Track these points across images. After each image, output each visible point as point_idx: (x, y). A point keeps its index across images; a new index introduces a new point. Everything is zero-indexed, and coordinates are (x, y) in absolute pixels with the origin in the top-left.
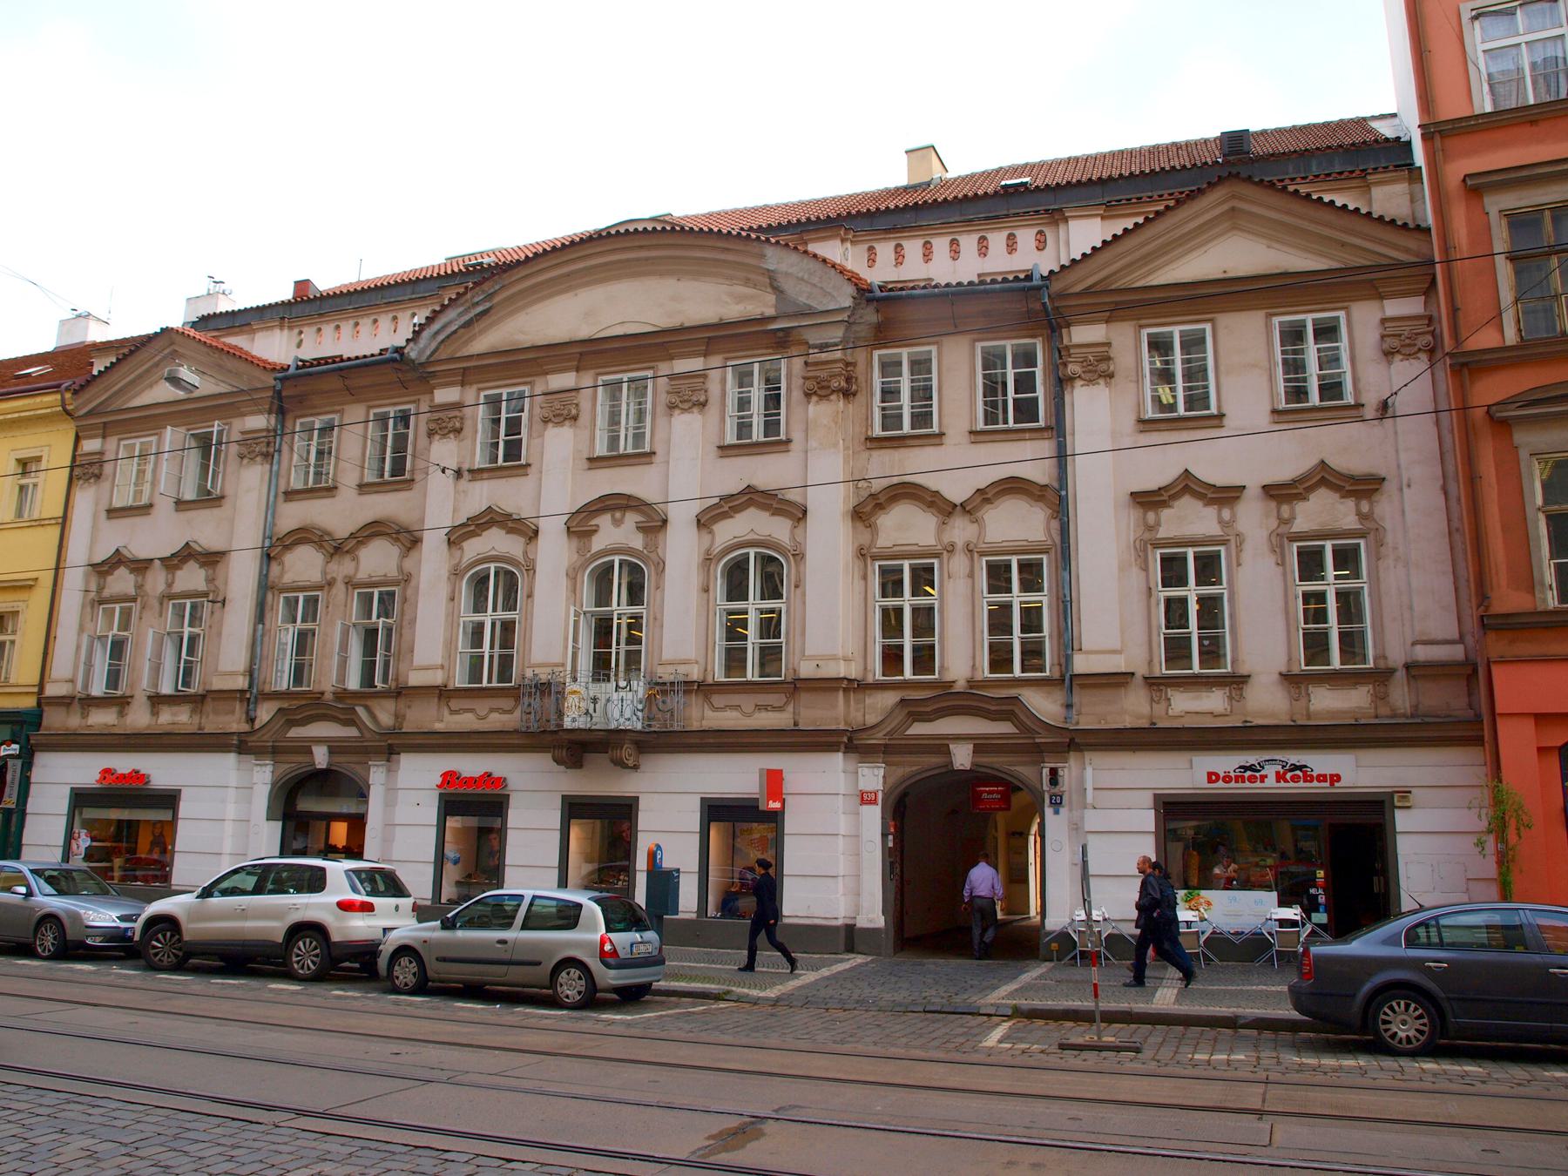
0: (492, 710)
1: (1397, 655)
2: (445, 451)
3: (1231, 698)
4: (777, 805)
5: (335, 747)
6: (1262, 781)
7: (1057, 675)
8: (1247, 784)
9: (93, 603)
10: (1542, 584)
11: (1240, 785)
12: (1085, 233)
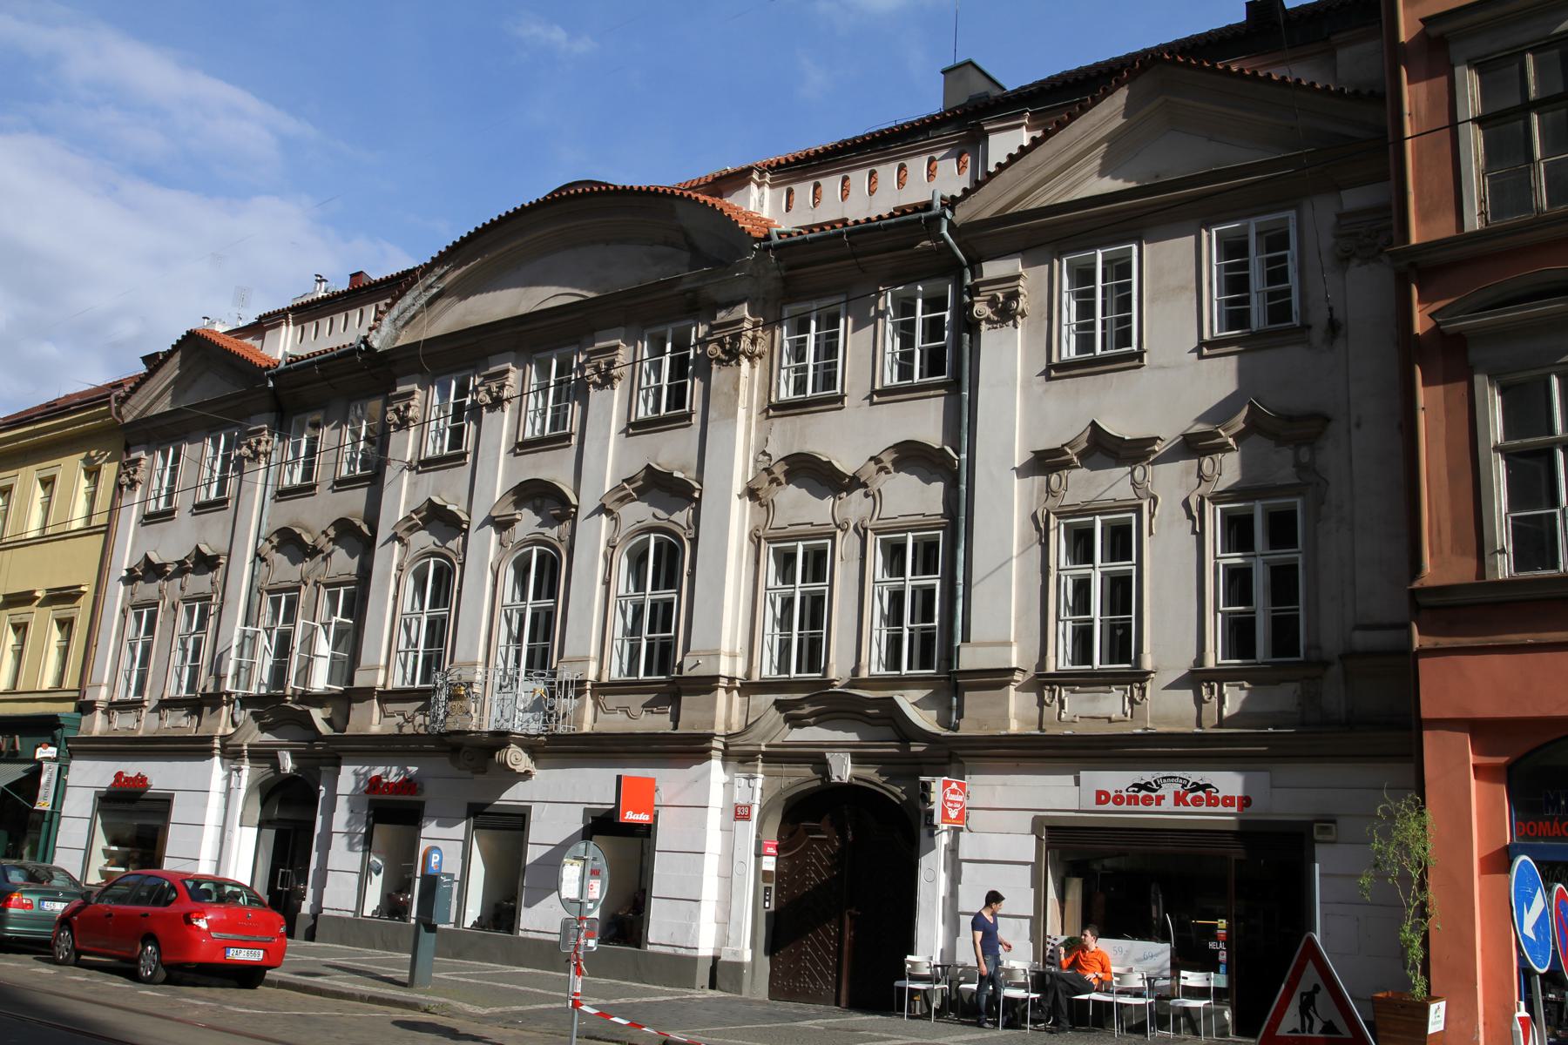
1: (1331, 644)
4: (644, 818)
6: (1158, 804)
8: (1141, 807)
11: (1133, 808)
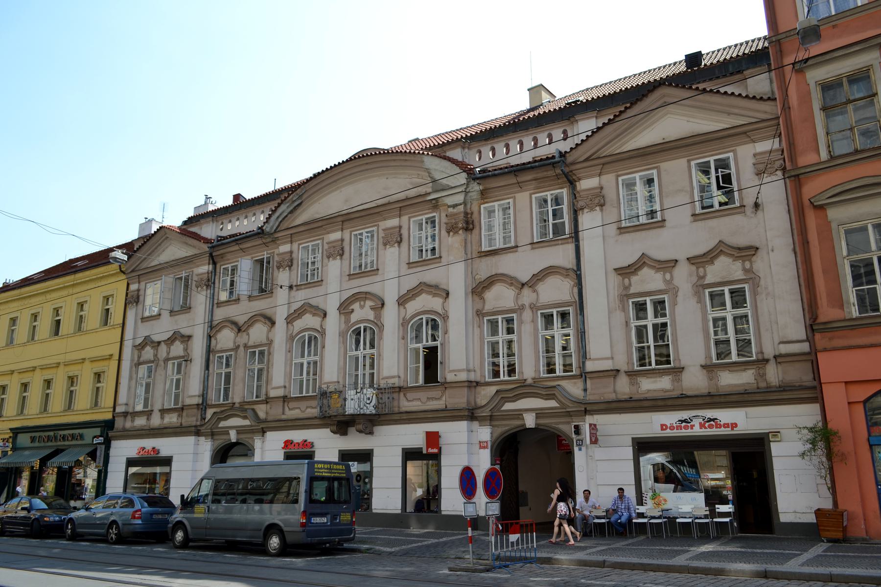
0: (307, 407)
1: (769, 352)
2: (283, 277)
3: (673, 381)
4: (435, 451)
5: (240, 430)
6: (692, 428)
7: (578, 373)
8: (683, 430)
9: (135, 365)
10: (848, 303)
12: (586, 125)
